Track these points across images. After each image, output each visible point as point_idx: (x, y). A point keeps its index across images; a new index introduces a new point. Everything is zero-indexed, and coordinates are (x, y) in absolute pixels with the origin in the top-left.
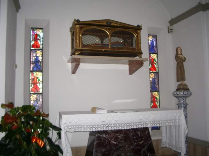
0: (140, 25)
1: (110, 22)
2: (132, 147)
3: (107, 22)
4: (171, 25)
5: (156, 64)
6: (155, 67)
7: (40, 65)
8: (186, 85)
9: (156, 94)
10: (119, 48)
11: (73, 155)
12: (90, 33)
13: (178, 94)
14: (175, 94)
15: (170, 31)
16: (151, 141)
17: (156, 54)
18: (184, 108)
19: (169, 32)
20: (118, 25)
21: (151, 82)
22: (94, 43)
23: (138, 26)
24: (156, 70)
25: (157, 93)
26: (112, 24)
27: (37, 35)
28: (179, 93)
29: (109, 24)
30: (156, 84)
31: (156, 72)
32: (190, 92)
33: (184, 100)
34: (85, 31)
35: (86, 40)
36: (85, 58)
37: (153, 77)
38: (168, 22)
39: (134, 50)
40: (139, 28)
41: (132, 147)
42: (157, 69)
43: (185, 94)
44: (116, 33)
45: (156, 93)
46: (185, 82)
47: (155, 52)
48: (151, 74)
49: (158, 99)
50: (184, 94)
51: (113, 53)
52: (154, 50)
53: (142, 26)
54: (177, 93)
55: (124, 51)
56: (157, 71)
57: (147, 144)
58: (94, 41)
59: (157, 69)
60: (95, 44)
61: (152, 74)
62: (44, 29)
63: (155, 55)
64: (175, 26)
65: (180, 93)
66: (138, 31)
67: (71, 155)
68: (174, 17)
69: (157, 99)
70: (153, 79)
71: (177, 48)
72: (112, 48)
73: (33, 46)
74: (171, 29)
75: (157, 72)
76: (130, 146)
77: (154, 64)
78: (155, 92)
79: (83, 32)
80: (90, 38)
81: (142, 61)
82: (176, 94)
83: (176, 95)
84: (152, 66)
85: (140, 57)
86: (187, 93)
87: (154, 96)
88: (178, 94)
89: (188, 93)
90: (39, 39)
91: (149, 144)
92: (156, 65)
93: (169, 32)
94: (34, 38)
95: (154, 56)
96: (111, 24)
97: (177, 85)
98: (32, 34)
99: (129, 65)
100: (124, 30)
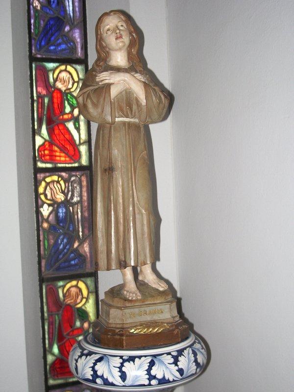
5: (76, 120)
6: (71, 140)
9: (80, 290)
11: (29, 391)
17: (78, 61)
21: (45, 225)
24: (76, 156)
25: (81, 285)
28: (117, 374)
31: (76, 165)
37: (60, 197)
42: (83, 149)
45: (76, 286)
47: (74, 49)
48: (48, 180)
49: (92, 316)
51: (101, 141)
52: (70, 40)
54: (101, 368)
56: (84, 161)
59: (83, 149)
61: (55, 178)
63: (69, 68)
65: (123, 376)
67: (27, 390)
69: (83, 315)
75: (81, 168)
77: (63, 122)
78: (74, 283)
84: (50, 132)
86: (174, 368)
87: (69, 301)
88: (106, 382)
89: (181, 371)
92: (78, 129)
95: (64, 75)
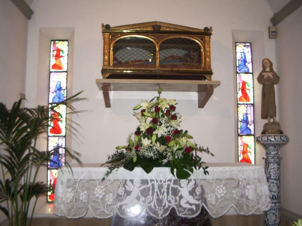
0: (209, 28)
1: (159, 26)
2: (174, 224)
3: (153, 27)
4: (274, 25)
7: (63, 95)
8: (278, 124)
10: (173, 66)
12: (172, 45)
13: (260, 140)
14: (266, 139)
15: (273, 34)
16: (208, 216)
18: (278, 165)
19: (270, 38)
20: (172, 29)
22: (132, 59)
23: (206, 29)
26: (162, 29)
27: (59, 51)
29: (156, 29)
30: (250, 123)
32: (285, 136)
33: (277, 150)
34: (163, 42)
35: (138, 55)
36: (115, 82)
38: (269, 20)
39: (198, 69)
40: (207, 33)
41: (174, 223)
43: (283, 141)
44: (175, 43)
46: (277, 119)
47: (248, 70)
50: (281, 139)
53: (213, 29)
54: (269, 138)
55: (180, 69)
57: (201, 221)
58: (121, 56)
60: (134, 60)
62: (69, 41)
64: (283, 25)
66: (207, 38)
68: (277, 10)
70: (245, 116)
71: (263, 61)
72: (161, 65)
73: (54, 66)
74: (273, 32)
76: (171, 222)
79: (161, 44)
80: (138, 51)
81: (212, 85)
82: (268, 139)
83: (268, 141)
85: (210, 79)
88: (271, 141)
90: (62, 56)
91: (203, 221)
93: (271, 36)
94: (55, 55)
96: (160, 28)
97: (264, 125)
98: (53, 49)
99: (198, 93)
100: (183, 37)
